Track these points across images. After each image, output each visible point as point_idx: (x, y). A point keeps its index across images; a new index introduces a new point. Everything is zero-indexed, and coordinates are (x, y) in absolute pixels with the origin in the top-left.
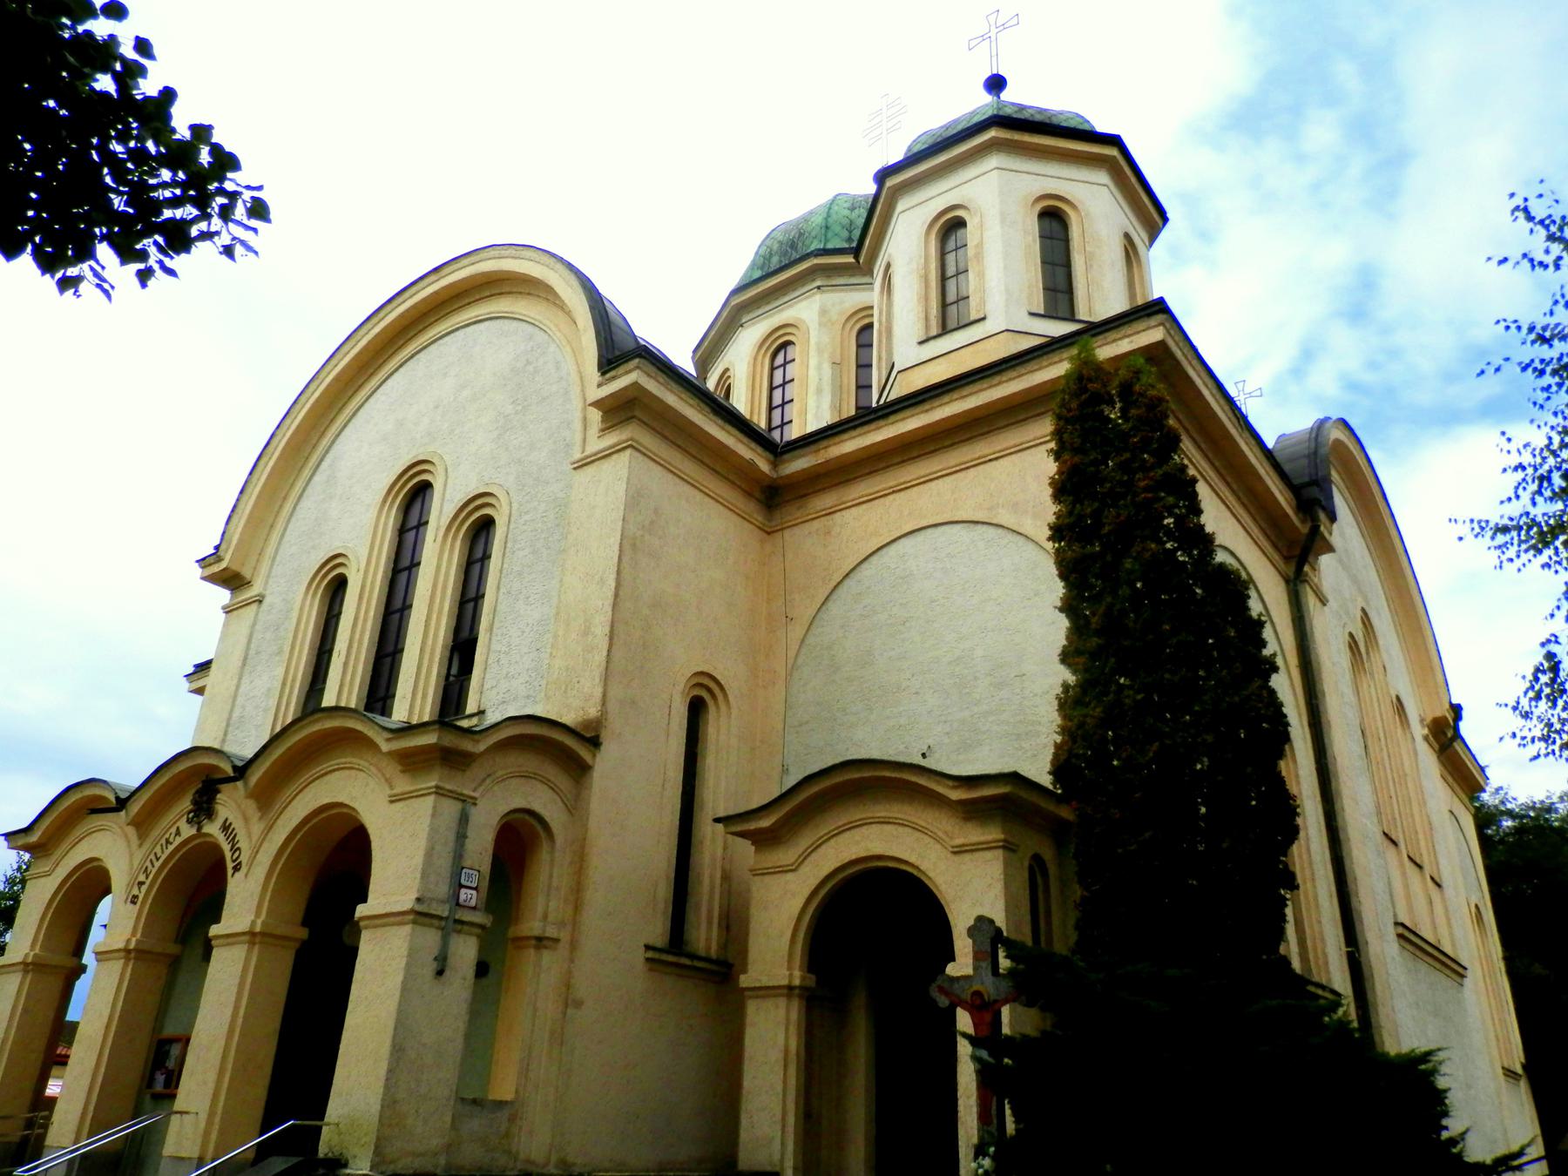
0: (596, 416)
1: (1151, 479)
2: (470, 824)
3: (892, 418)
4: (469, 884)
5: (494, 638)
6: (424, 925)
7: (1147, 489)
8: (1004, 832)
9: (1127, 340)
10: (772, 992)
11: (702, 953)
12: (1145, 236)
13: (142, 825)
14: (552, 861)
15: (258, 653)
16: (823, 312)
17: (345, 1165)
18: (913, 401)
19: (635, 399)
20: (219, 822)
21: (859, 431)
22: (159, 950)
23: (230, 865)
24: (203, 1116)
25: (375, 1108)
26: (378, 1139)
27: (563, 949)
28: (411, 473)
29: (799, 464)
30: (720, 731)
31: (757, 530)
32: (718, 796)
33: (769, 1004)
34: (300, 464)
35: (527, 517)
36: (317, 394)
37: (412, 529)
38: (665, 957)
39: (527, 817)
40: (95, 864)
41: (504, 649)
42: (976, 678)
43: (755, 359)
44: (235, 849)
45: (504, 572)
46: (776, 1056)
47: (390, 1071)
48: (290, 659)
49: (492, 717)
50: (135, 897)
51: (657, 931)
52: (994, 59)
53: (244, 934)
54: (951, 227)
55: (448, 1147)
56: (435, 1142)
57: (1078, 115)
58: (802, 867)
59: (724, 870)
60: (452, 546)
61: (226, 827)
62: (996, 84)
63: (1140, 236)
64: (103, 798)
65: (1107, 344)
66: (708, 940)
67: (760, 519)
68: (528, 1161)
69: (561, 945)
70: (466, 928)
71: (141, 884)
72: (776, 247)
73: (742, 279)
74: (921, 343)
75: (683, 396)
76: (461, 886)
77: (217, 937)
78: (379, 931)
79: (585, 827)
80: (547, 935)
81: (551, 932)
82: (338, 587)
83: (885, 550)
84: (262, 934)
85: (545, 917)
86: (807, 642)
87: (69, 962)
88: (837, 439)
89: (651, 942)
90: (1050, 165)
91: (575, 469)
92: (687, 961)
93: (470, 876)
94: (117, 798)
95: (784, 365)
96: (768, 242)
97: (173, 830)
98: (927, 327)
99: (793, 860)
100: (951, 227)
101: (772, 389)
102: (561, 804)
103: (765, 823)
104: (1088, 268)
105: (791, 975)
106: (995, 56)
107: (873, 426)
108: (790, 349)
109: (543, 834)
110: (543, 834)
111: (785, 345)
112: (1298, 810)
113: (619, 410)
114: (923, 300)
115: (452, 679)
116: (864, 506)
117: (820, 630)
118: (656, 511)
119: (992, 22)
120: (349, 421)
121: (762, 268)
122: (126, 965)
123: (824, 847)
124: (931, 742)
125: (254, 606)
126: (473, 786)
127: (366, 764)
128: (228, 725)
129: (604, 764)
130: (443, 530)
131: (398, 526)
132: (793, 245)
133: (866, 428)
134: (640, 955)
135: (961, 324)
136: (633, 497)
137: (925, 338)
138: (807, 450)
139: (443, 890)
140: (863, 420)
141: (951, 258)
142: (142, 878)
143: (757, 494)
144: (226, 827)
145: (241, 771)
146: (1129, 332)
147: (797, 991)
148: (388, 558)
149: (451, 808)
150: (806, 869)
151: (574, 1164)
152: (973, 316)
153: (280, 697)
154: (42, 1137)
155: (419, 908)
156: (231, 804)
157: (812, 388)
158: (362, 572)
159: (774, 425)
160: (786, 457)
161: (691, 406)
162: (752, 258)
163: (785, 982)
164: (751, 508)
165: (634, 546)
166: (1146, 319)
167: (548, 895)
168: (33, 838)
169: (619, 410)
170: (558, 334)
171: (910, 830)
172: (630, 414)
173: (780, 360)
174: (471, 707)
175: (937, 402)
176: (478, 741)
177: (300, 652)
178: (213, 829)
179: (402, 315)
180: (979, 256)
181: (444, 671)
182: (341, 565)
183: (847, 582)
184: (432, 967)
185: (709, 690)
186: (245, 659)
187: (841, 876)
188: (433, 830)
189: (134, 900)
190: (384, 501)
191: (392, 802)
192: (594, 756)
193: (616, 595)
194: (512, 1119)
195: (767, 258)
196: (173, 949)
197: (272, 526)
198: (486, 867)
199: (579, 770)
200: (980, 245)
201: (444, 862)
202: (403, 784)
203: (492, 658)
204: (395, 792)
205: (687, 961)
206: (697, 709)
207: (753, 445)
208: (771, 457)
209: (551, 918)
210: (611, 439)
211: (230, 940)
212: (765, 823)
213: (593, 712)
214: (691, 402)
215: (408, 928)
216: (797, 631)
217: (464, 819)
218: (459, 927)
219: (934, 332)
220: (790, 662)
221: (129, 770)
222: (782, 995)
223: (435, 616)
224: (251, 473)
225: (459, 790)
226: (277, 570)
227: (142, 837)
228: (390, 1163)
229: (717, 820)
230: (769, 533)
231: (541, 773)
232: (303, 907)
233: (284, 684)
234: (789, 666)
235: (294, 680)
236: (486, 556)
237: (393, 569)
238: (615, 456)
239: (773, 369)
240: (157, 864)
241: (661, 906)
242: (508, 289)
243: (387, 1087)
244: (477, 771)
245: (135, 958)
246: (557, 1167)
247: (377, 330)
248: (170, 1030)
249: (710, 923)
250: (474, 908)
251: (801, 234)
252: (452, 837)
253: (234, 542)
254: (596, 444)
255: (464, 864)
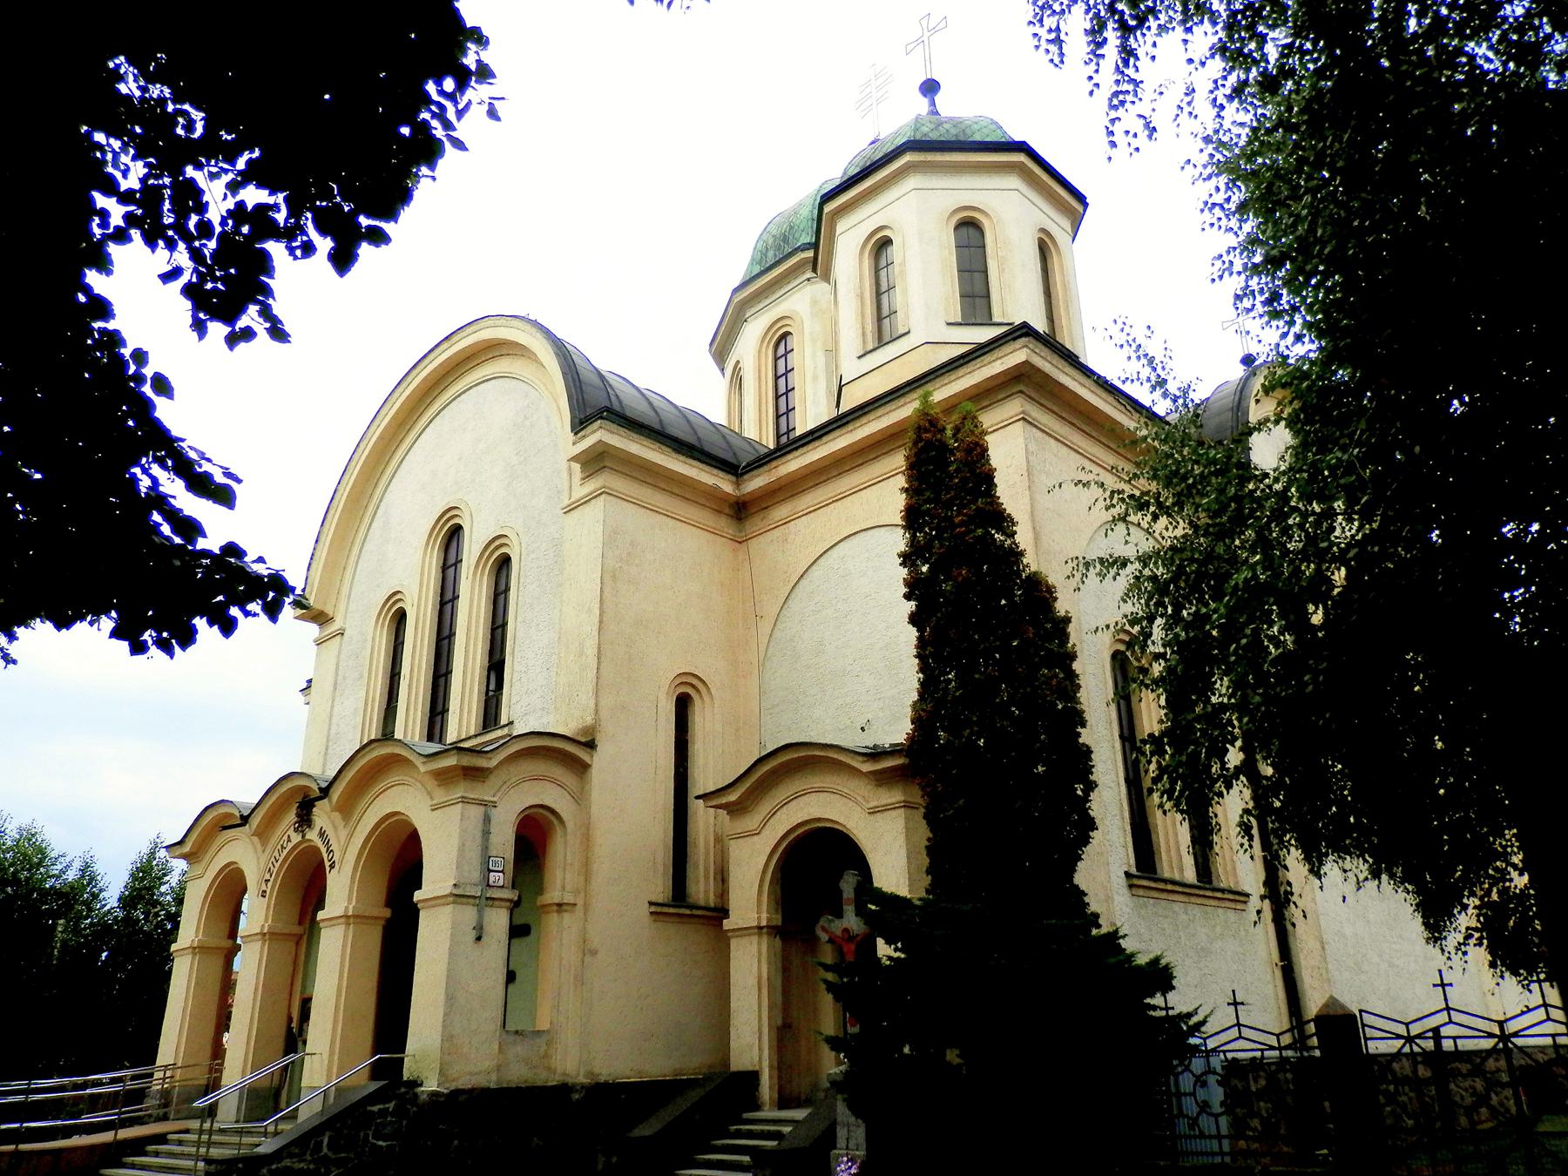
0: (577, 467)
1: (965, 515)
2: (493, 823)
3: (825, 439)
4: (496, 869)
5: (516, 660)
6: (461, 904)
7: (962, 524)
8: (905, 793)
9: (999, 362)
10: (745, 932)
11: (702, 903)
12: (1067, 224)
13: (263, 834)
14: (565, 843)
15: (344, 678)
16: (814, 302)
17: (421, 1085)
18: (839, 423)
19: (604, 452)
20: (317, 829)
21: (800, 451)
22: (286, 931)
23: (327, 864)
24: (326, 1056)
25: (438, 1043)
26: (441, 1064)
27: (579, 908)
28: (445, 518)
29: (757, 482)
30: (703, 721)
31: (730, 542)
32: (708, 773)
33: (745, 941)
34: (361, 513)
35: (533, 556)
36: (366, 453)
37: (451, 566)
38: (666, 910)
39: (541, 811)
40: (235, 866)
41: (524, 669)
42: (901, 661)
43: (760, 351)
44: (330, 851)
45: (520, 603)
46: (753, 981)
47: (446, 1015)
48: (368, 684)
49: (518, 730)
50: (265, 892)
51: (661, 888)
52: (928, 63)
53: (257, 934)
54: (781, 341)
55: (499, 1068)
56: (487, 1064)
57: (994, 122)
58: (764, 830)
59: (716, 835)
60: (481, 581)
61: (322, 834)
62: (930, 88)
63: (1059, 226)
64: (231, 815)
65: (985, 365)
66: (706, 892)
67: (730, 531)
68: (564, 1074)
69: (577, 907)
70: (497, 903)
71: (267, 881)
72: (771, 241)
73: (745, 275)
74: (859, 357)
75: (645, 443)
76: (490, 871)
77: (323, 920)
78: (432, 911)
79: (589, 813)
80: (565, 901)
81: (568, 898)
82: (401, 617)
83: (829, 553)
84: (353, 916)
85: (563, 888)
86: (774, 636)
87: (228, 943)
88: (784, 459)
89: (654, 899)
90: (964, 178)
91: (565, 513)
92: (688, 912)
93: (495, 863)
94: (241, 816)
95: (785, 355)
96: (765, 237)
97: (285, 838)
98: (864, 342)
99: (755, 827)
100: (781, 341)
101: (777, 378)
102: (569, 797)
103: (733, 797)
104: (1001, 271)
105: (759, 918)
106: (928, 60)
107: (810, 446)
108: (789, 338)
109: (556, 822)
110: (556, 822)
111: (785, 336)
112: (1094, 770)
113: (595, 462)
114: (860, 318)
115: (491, 693)
116: (812, 514)
117: (783, 625)
118: (632, 543)
119: (925, 27)
120: (395, 472)
121: (760, 263)
122: (263, 945)
123: (778, 813)
124: (870, 716)
125: (338, 637)
126: (492, 793)
127: (413, 781)
128: (328, 741)
129: (599, 761)
130: (472, 568)
131: (441, 564)
132: (785, 239)
133: (805, 449)
134: (645, 910)
135: (894, 337)
136: (610, 535)
137: (862, 353)
138: (761, 470)
139: (476, 875)
140: (804, 441)
141: (883, 273)
142: (267, 877)
143: (727, 510)
144: (322, 834)
145: (325, 792)
146: (1000, 355)
147: (765, 930)
148: (435, 593)
149: (476, 812)
150: (766, 832)
151: (600, 1074)
152: (902, 331)
153: (364, 716)
154: (220, 1078)
155: (456, 892)
156: (322, 815)
157: (808, 379)
158: (415, 607)
159: (781, 413)
160: (745, 477)
161: (654, 450)
162: (751, 254)
163: (755, 924)
164: (724, 524)
165: (614, 577)
166: (1012, 342)
167: (565, 870)
168: (187, 848)
169: (595, 462)
170: (546, 392)
171: (795, 801)
172: (602, 465)
173: (781, 350)
174: (504, 721)
175: (858, 423)
176: (491, 759)
177: (376, 675)
178: (312, 835)
179: (425, 379)
180: (902, 272)
181: (484, 689)
182: (400, 600)
183: (803, 582)
184: (473, 934)
185: (693, 686)
186: (335, 684)
187: (792, 837)
188: (463, 831)
189: (264, 894)
190: (427, 544)
191: (433, 810)
192: (592, 756)
193: (601, 622)
194: (549, 1043)
195: (764, 254)
196: (297, 930)
197: (344, 568)
198: (510, 854)
199: (582, 768)
200: (903, 263)
201: (474, 855)
202: (440, 795)
203: (516, 675)
204: (434, 802)
205: (688, 912)
206: (683, 705)
207: (715, 471)
208: (734, 478)
209: (568, 888)
210: (591, 486)
211: (331, 923)
212: (733, 797)
213: (589, 720)
214: (652, 446)
215: (449, 908)
216: (766, 627)
217: (487, 820)
218: (490, 903)
219: (870, 347)
220: (762, 654)
221: (247, 794)
222: (754, 934)
223: (472, 642)
224: (322, 525)
225: (481, 798)
226: (352, 607)
227: (264, 843)
228: (453, 1081)
229: (698, 797)
230: (740, 543)
231: (549, 775)
232: (384, 891)
233: (366, 704)
234: (761, 658)
235: (373, 701)
236: (507, 589)
237: (441, 601)
238: (593, 501)
239: (776, 359)
240: (277, 865)
241: (661, 869)
242: (505, 352)
243: (444, 1027)
244: (494, 781)
245: (270, 939)
246: (585, 1077)
247: (408, 392)
248: (306, 996)
249: (707, 877)
250: (503, 887)
251: (791, 228)
252: (479, 835)
253: (316, 585)
254: (580, 491)
255: (493, 853)
